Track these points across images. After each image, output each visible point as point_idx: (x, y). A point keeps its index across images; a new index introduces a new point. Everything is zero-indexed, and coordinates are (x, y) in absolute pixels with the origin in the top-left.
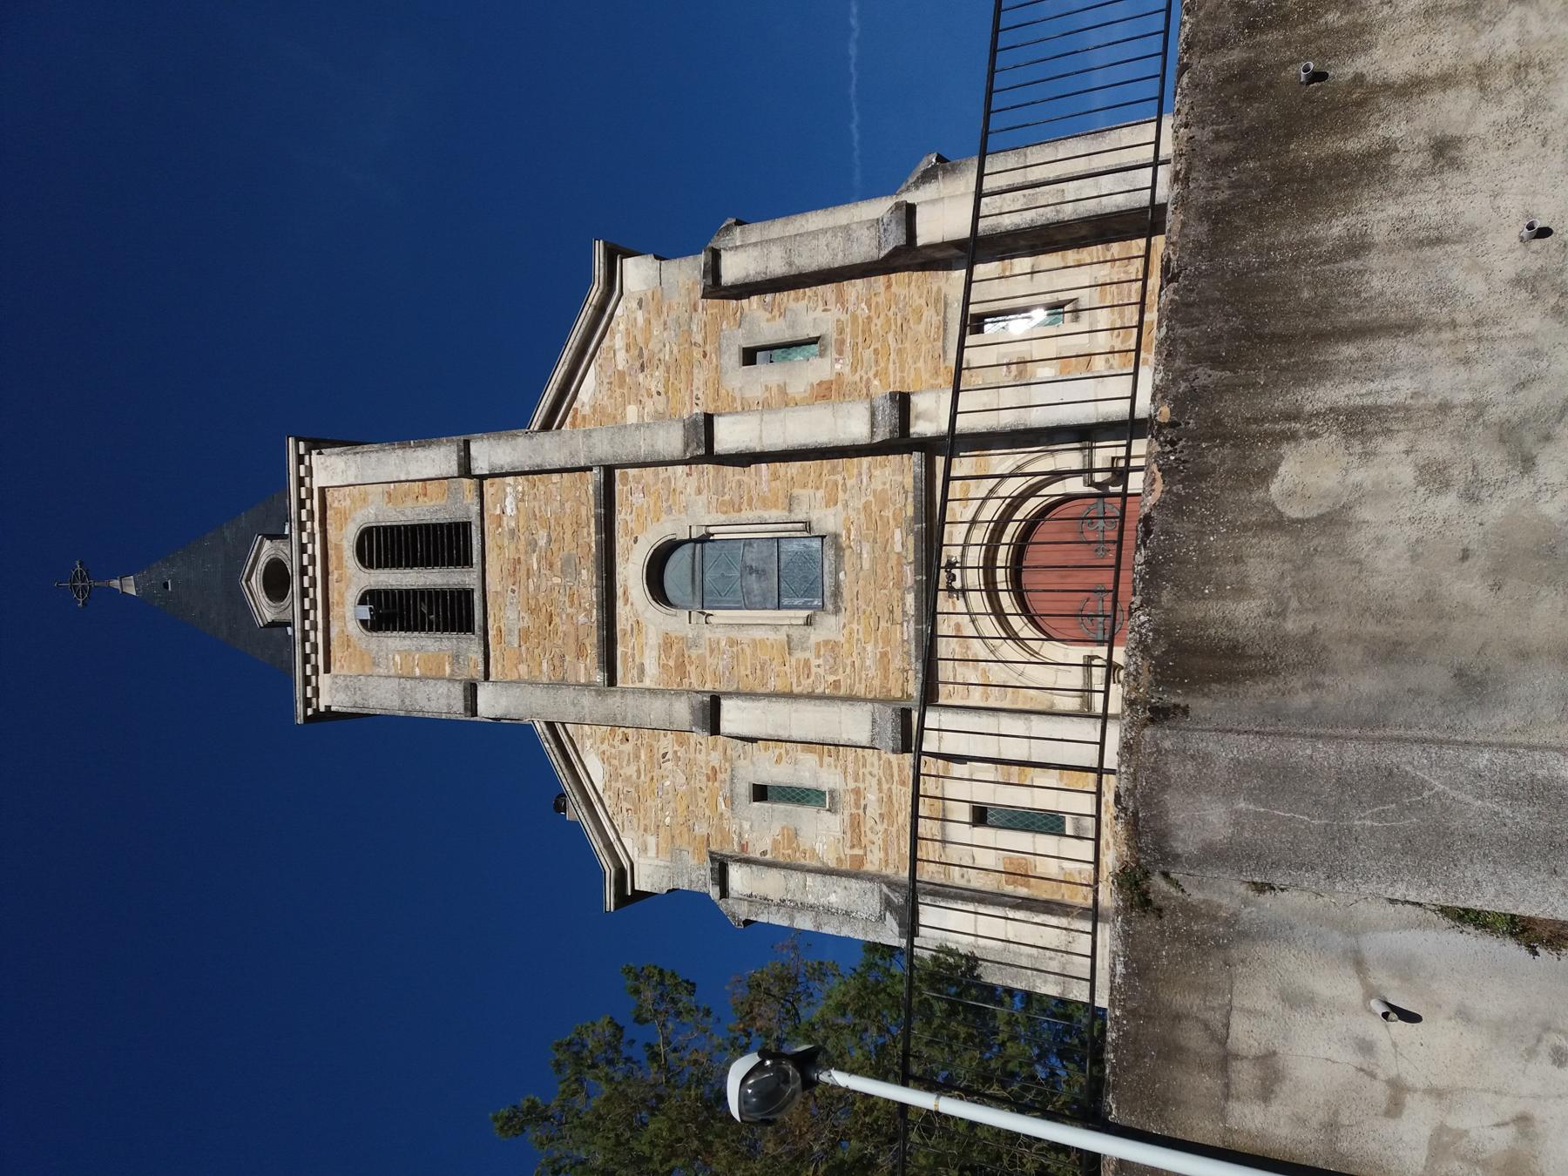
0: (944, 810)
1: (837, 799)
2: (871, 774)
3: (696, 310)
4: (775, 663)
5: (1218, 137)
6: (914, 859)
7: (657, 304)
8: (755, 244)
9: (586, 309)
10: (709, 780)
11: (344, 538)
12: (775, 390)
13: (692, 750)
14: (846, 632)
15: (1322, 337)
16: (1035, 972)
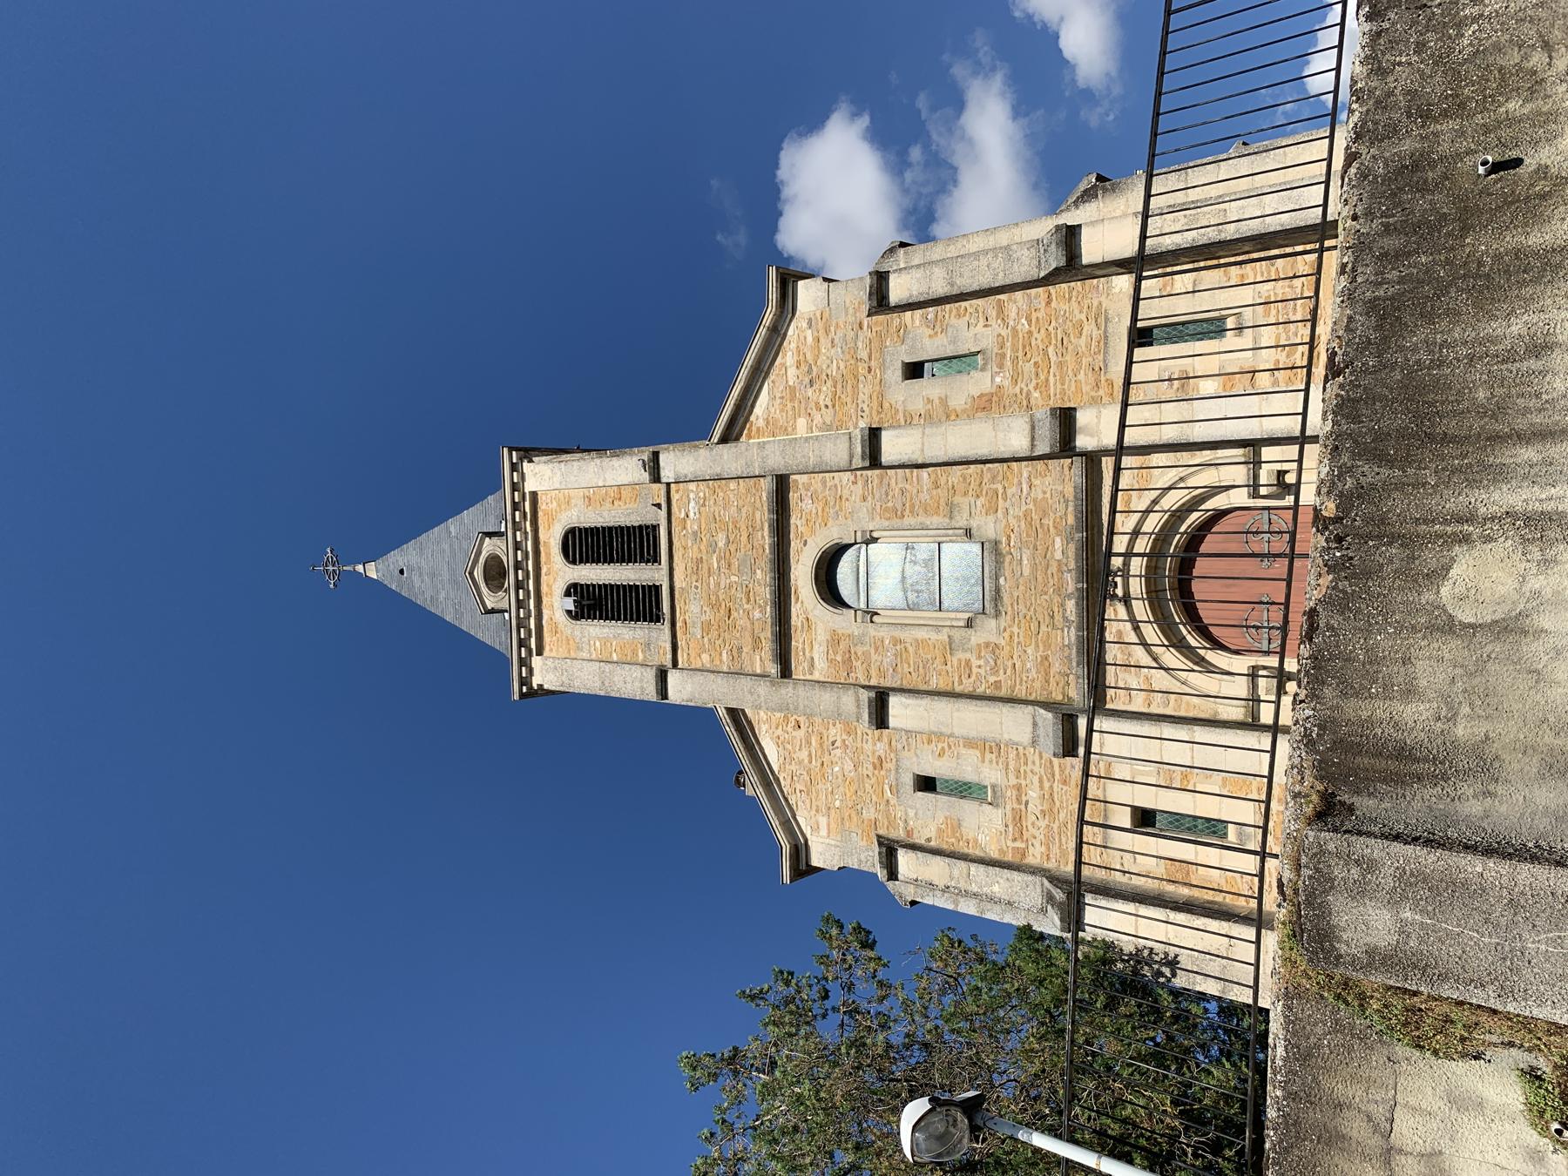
1: (999, 794)
3: (861, 328)
5: (1387, 230)
7: (826, 323)
8: (918, 266)
9: (760, 330)
10: (875, 769)
11: (552, 538)
12: (937, 401)
14: (1006, 635)
15: (1496, 439)
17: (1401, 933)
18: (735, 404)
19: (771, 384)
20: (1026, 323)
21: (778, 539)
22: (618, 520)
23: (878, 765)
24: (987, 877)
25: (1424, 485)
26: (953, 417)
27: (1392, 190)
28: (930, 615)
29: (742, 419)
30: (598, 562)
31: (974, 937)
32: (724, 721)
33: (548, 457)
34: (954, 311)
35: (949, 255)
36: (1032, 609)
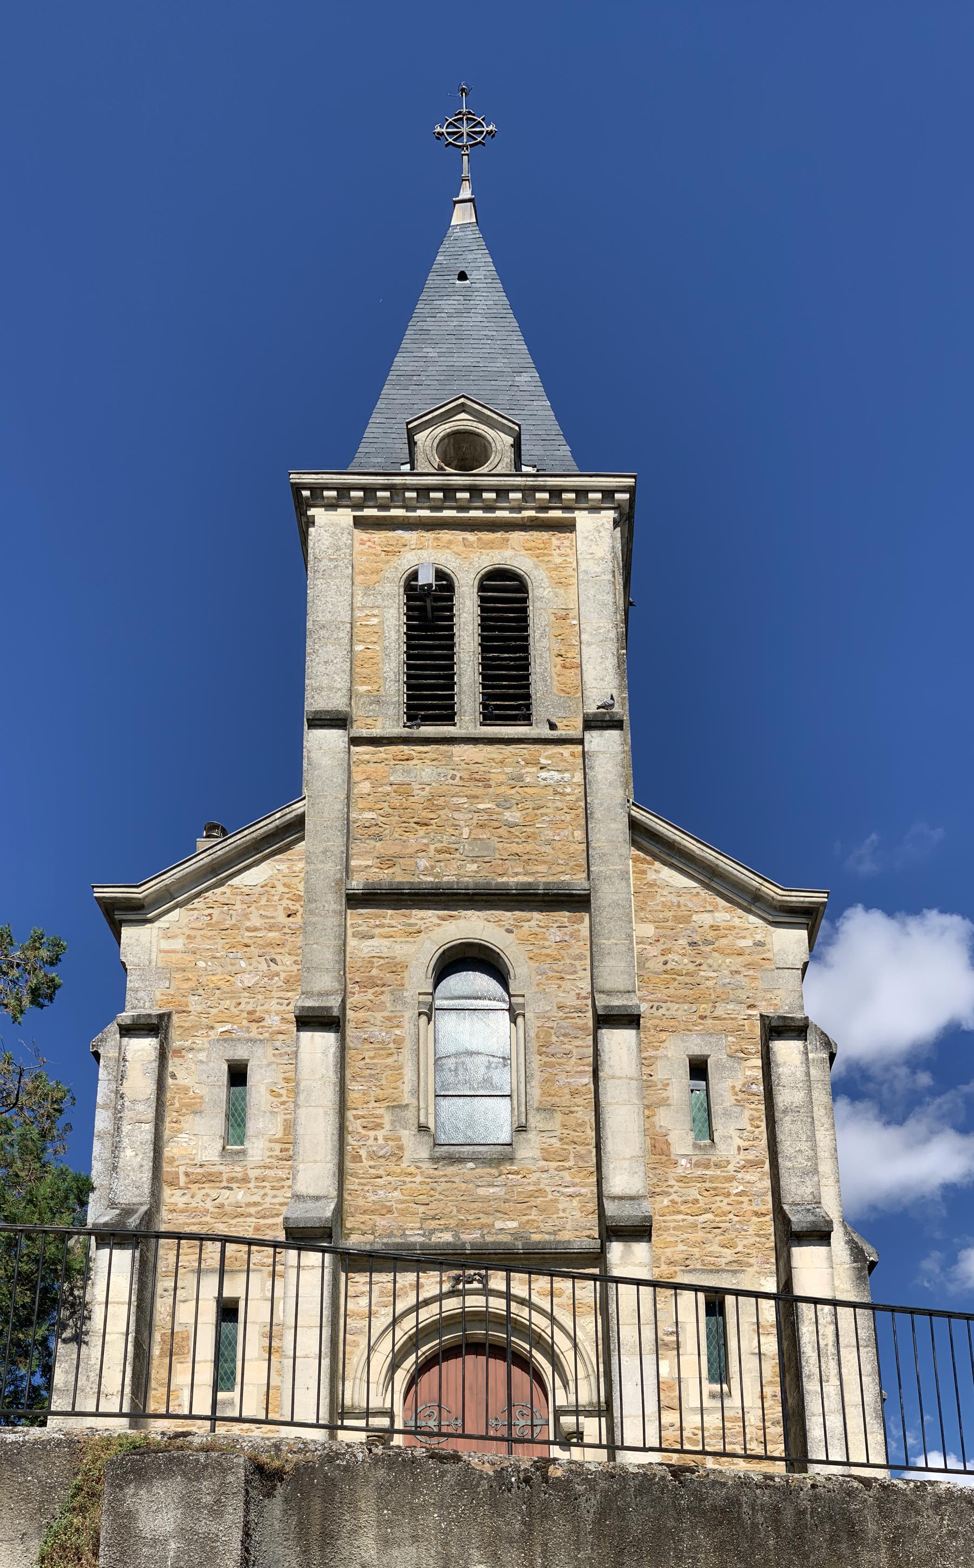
0: (232, 1271)
1: (236, 1158)
2: (265, 1194)
4: (379, 1091)
6: (179, 1236)
7: (758, 964)
8: (808, 1074)
12: (665, 1094)
13: (282, 994)
16: (75, 1362)
17: (155, 1540)
18: (674, 841)
19: (695, 891)
20: (739, 1190)
21: (514, 895)
22: (538, 661)
23: (253, 1017)
24: (141, 1143)
25: (578, 1549)
26: (647, 1112)
27: (835, 1516)
28: (430, 1084)
29: (657, 851)
30: (483, 627)
31: (69, 1127)
32: (287, 810)
33: (621, 559)
34: (756, 1114)
35: (815, 1109)
36: (442, 1197)
